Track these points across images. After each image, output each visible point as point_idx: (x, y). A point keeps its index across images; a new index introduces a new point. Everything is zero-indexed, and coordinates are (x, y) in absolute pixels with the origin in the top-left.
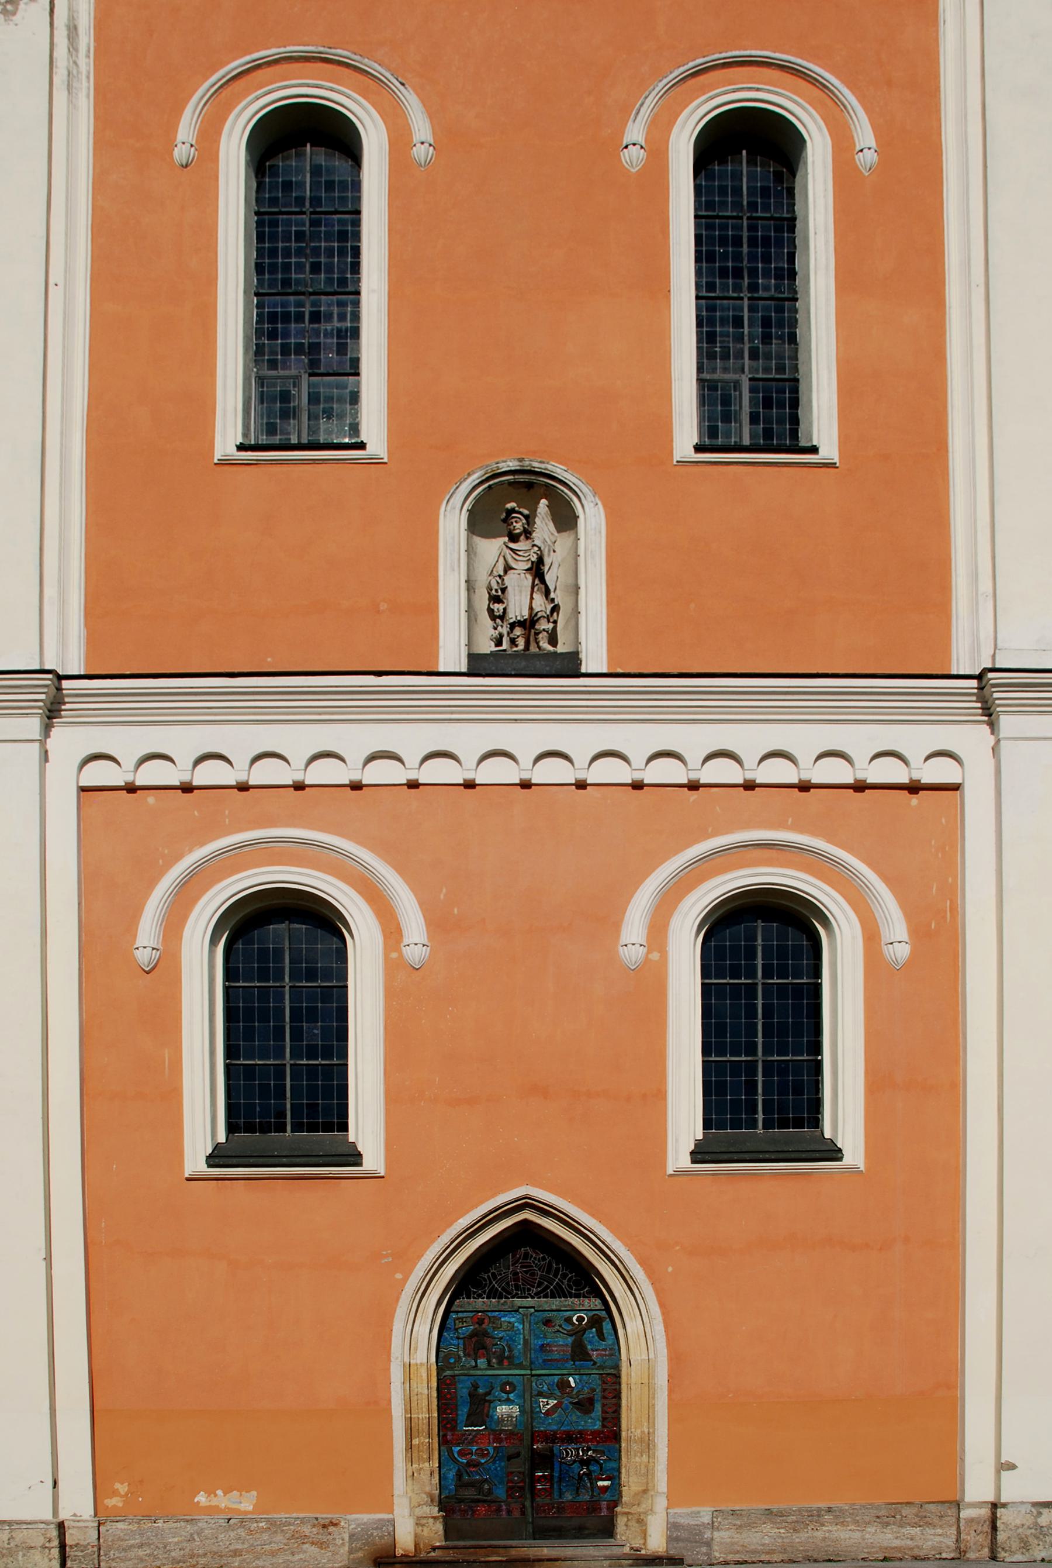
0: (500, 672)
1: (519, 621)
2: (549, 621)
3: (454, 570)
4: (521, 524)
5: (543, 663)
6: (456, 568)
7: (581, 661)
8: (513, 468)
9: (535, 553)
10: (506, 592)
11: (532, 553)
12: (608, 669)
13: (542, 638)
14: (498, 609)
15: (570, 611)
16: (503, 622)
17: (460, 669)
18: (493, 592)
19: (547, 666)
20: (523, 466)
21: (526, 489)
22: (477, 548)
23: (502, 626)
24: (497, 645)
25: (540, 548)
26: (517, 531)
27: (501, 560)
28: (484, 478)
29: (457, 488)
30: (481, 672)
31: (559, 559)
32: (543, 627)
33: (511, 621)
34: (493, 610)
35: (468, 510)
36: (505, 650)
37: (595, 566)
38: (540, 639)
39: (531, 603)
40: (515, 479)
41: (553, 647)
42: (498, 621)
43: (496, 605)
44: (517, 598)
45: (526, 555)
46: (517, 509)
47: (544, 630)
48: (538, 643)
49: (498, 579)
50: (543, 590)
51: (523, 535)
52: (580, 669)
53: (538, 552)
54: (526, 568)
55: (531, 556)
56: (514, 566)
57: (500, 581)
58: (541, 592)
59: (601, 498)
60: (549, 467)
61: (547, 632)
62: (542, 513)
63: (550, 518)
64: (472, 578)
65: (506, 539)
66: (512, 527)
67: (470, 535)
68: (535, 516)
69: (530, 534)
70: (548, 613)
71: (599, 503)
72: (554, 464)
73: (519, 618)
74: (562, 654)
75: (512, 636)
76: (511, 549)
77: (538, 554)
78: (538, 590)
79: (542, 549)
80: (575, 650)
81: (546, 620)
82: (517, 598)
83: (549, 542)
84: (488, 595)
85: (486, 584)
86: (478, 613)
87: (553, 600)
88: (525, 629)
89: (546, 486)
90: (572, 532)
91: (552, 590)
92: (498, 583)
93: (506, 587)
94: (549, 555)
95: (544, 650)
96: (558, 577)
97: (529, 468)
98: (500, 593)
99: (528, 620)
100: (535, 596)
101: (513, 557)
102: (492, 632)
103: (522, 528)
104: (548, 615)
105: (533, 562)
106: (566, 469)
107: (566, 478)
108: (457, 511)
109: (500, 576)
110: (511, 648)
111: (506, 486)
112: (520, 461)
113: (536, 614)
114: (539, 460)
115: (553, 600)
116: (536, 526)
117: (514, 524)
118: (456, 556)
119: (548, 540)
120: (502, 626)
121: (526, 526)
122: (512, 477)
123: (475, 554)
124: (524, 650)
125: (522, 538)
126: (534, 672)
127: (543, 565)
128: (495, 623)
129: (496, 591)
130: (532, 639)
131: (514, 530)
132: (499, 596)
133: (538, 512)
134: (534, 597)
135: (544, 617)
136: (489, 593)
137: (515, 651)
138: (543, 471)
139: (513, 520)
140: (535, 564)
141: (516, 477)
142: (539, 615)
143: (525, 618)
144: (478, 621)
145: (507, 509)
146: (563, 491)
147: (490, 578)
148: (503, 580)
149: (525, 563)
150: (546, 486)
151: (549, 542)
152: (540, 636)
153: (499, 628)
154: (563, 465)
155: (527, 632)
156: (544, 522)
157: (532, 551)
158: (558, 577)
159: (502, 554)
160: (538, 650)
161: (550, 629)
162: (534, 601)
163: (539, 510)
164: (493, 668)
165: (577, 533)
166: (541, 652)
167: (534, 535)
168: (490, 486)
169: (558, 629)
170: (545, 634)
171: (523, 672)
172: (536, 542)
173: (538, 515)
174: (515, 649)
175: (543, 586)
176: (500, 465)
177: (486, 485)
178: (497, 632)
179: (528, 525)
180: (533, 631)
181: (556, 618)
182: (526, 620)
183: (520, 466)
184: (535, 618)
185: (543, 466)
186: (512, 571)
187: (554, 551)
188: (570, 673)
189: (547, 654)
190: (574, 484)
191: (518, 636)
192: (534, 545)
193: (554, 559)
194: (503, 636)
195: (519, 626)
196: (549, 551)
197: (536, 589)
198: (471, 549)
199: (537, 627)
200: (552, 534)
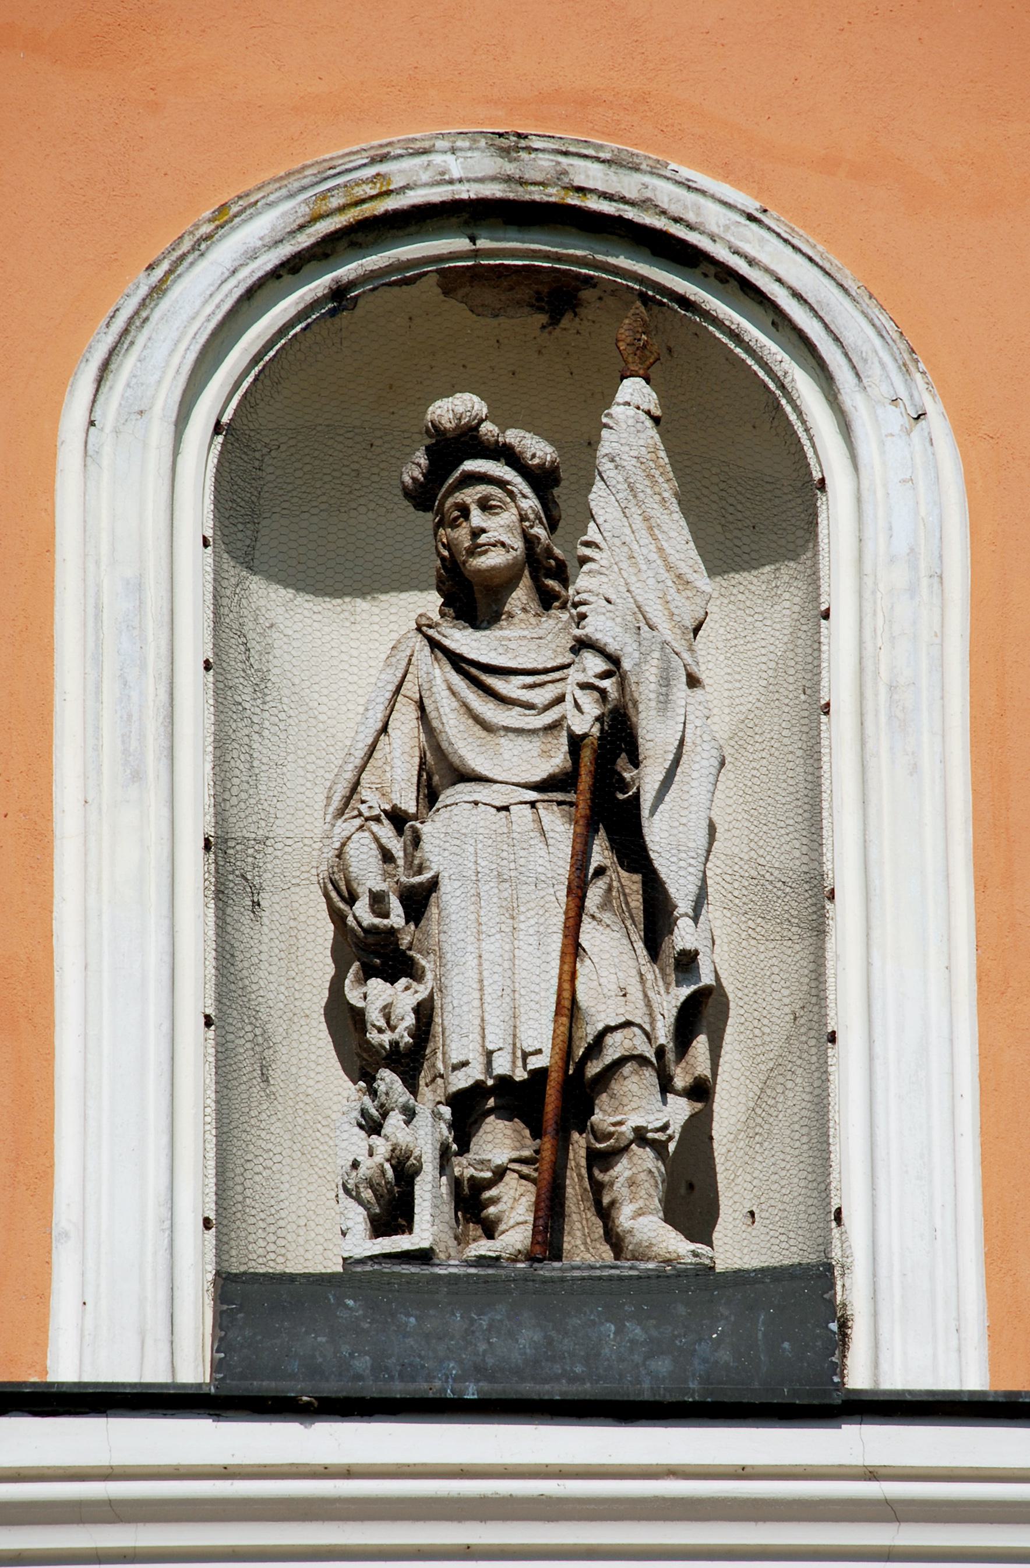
0: (398, 1389)
1: (505, 1082)
2: (666, 1086)
3: (137, 776)
4: (509, 516)
5: (635, 1331)
6: (153, 764)
7: (844, 1325)
8: (466, 192)
9: (584, 686)
10: (433, 911)
11: (570, 688)
12: (994, 1365)
13: (632, 1183)
14: (387, 1012)
15: (779, 1024)
16: (412, 1087)
17: (80, 1376)
18: (362, 910)
19: (656, 1348)
20: (522, 182)
21: (543, 318)
22: (268, 649)
23: (410, 1114)
24: (380, 1227)
25: (614, 660)
26: (494, 559)
27: (405, 718)
28: (305, 240)
29: (158, 290)
30: (290, 1388)
31: (721, 725)
32: (635, 1120)
33: (461, 1081)
34: (358, 1016)
35: (218, 428)
36: (424, 1256)
37: (915, 769)
38: (620, 1190)
39: (569, 978)
40: (476, 254)
41: (692, 1238)
42: (388, 1080)
43: (376, 984)
44: (492, 946)
45: (541, 697)
46: (488, 429)
47: (640, 1136)
48: (605, 1213)
49: (386, 831)
50: (636, 902)
51: (526, 581)
52: (840, 1368)
53: (606, 684)
54: (541, 771)
55: (568, 704)
56: (477, 762)
57: (396, 846)
58: (624, 913)
59: (943, 388)
60: (665, 193)
61: (659, 1148)
62: (629, 463)
63: (668, 490)
64: (243, 828)
65: (431, 602)
66: (462, 535)
67: (233, 571)
68: (589, 475)
69: (562, 575)
70: (663, 1034)
71: (938, 422)
72: (686, 172)
73: (502, 1066)
74: (740, 1278)
75: (464, 1168)
76: (458, 662)
77: (603, 692)
78: (606, 904)
79: (626, 665)
80: (812, 1258)
81: (650, 1076)
82: (492, 946)
83: (666, 631)
84: (329, 929)
85: (322, 861)
86: (277, 1028)
87: (687, 963)
88: (537, 1133)
89: (643, 297)
90: (788, 569)
91: (683, 905)
92: (387, 857)
93: (434, 884)
94: (665, 702)
95: (639, 1256)
96: (712, 829)
97: (553, 195)
98: (397, 917)
99: (554, 1079)
100: (590, 935)
101: (465, 705)
102: (357, 1142)
103: (518, 544)
104: (660, 1052)
105: (576, 742)
106: (752, 205)
107: (751, 262)
108: (160, 430)
109: (398, 818)
110: (461, 1240)
111: (430, 287)
112: (505, 152)
113: (597, 1046)
114: (611, 146)
115: (687, 963)
116: (592, 533)
117: (477, 518)
118: (154, 693)
119: (656, 613)
120: (410, 1114)
121: (539, 531)
122: (460, 244)
123: (261, 686)
124: (531, 1257)
125: (521, 596)
126: (586, 1390)
127: (635, 763)
128: (373, 1093)
129: (378, 901)
130: (574, 1187)
131: (474, 551)
132: (392, 932)
133: (604, 448)
134: (584, 940)
135: (642, 1060)
136: (338, 917)
137: (481, 1261)
138: (630, 214)
139: (470, 495)
140: (587, 756)
141: (483, 243)
142: (616, 1046)
143: (536, 1063)
144: (276, 1075)
145: (437, 430)
146: (736, 337)
147: (346, 827)
148: (416, 840)
149: (532, 746)
150: (643, 297)
151: (666, 631)
152: (622, 1170)
153: (395, 1121)
154: (736, 183)
155: (547, 1144)
156: (634, 510)
157: (574, 675)
158: (712, 829)
159: (410, 689)
160: (607, 1253)
161: (675, 1129)
162: (583, 969)
163: (609, 443)
164: (362, 1364)
165: (814, 579)
166: (626, 1268)
167: (583, 582)
168: (339, 293)
169: (719, 1130)
170: (645, 1158)
171: (529, 1389)
172: (597, 627)
173: (606, 466)
174: (483, 1247)
175: (632, 883)
176: (398, 171)
177: (319, 285)
178: (382, 1147)
179: (552, 526)
180: (579, 1143)
181: (703, 1068)
182: (540, 1075)
183: (508, 179)
184: (593, 1069)
185: (629, 184)
186: (464, 791)
187: (693, 682)
188: (785, 1395)
189: (659, 1276)
190: (797, 295)
191: (500, 1173)
192: (582, 645)
193: (694, 722)
194: (417, 1171)
195: (505, 1112)
196: (666, 682)
197: (594, 895)
198: (235, 653)
199: (600, 1118)
200: (682, 582)
